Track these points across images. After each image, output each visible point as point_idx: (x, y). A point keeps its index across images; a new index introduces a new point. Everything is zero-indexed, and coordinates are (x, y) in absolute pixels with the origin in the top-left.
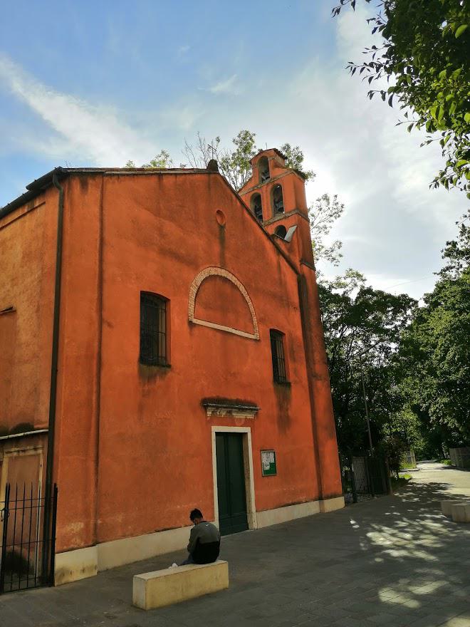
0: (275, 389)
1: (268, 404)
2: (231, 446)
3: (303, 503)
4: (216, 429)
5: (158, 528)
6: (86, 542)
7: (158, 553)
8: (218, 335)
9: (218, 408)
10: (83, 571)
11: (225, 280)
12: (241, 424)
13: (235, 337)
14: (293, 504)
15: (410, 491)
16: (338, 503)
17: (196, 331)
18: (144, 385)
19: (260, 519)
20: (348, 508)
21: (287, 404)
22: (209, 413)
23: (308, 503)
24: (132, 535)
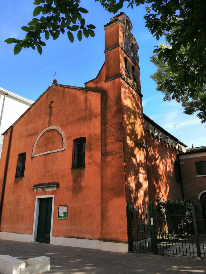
1: (67, 182)
2: (45, 204)
3: (86, 239)
4: (38, 197)
7: (13, 240)
11: (44, 133)
12: (49, 194)
13: (51, 154)
14: (78, 238)
15: (137, 179)
16: (123, 248)
17: (34, 159)
19: (55, 241)
21: (80, 179)
23: (92, 241)
24: (7, 232)
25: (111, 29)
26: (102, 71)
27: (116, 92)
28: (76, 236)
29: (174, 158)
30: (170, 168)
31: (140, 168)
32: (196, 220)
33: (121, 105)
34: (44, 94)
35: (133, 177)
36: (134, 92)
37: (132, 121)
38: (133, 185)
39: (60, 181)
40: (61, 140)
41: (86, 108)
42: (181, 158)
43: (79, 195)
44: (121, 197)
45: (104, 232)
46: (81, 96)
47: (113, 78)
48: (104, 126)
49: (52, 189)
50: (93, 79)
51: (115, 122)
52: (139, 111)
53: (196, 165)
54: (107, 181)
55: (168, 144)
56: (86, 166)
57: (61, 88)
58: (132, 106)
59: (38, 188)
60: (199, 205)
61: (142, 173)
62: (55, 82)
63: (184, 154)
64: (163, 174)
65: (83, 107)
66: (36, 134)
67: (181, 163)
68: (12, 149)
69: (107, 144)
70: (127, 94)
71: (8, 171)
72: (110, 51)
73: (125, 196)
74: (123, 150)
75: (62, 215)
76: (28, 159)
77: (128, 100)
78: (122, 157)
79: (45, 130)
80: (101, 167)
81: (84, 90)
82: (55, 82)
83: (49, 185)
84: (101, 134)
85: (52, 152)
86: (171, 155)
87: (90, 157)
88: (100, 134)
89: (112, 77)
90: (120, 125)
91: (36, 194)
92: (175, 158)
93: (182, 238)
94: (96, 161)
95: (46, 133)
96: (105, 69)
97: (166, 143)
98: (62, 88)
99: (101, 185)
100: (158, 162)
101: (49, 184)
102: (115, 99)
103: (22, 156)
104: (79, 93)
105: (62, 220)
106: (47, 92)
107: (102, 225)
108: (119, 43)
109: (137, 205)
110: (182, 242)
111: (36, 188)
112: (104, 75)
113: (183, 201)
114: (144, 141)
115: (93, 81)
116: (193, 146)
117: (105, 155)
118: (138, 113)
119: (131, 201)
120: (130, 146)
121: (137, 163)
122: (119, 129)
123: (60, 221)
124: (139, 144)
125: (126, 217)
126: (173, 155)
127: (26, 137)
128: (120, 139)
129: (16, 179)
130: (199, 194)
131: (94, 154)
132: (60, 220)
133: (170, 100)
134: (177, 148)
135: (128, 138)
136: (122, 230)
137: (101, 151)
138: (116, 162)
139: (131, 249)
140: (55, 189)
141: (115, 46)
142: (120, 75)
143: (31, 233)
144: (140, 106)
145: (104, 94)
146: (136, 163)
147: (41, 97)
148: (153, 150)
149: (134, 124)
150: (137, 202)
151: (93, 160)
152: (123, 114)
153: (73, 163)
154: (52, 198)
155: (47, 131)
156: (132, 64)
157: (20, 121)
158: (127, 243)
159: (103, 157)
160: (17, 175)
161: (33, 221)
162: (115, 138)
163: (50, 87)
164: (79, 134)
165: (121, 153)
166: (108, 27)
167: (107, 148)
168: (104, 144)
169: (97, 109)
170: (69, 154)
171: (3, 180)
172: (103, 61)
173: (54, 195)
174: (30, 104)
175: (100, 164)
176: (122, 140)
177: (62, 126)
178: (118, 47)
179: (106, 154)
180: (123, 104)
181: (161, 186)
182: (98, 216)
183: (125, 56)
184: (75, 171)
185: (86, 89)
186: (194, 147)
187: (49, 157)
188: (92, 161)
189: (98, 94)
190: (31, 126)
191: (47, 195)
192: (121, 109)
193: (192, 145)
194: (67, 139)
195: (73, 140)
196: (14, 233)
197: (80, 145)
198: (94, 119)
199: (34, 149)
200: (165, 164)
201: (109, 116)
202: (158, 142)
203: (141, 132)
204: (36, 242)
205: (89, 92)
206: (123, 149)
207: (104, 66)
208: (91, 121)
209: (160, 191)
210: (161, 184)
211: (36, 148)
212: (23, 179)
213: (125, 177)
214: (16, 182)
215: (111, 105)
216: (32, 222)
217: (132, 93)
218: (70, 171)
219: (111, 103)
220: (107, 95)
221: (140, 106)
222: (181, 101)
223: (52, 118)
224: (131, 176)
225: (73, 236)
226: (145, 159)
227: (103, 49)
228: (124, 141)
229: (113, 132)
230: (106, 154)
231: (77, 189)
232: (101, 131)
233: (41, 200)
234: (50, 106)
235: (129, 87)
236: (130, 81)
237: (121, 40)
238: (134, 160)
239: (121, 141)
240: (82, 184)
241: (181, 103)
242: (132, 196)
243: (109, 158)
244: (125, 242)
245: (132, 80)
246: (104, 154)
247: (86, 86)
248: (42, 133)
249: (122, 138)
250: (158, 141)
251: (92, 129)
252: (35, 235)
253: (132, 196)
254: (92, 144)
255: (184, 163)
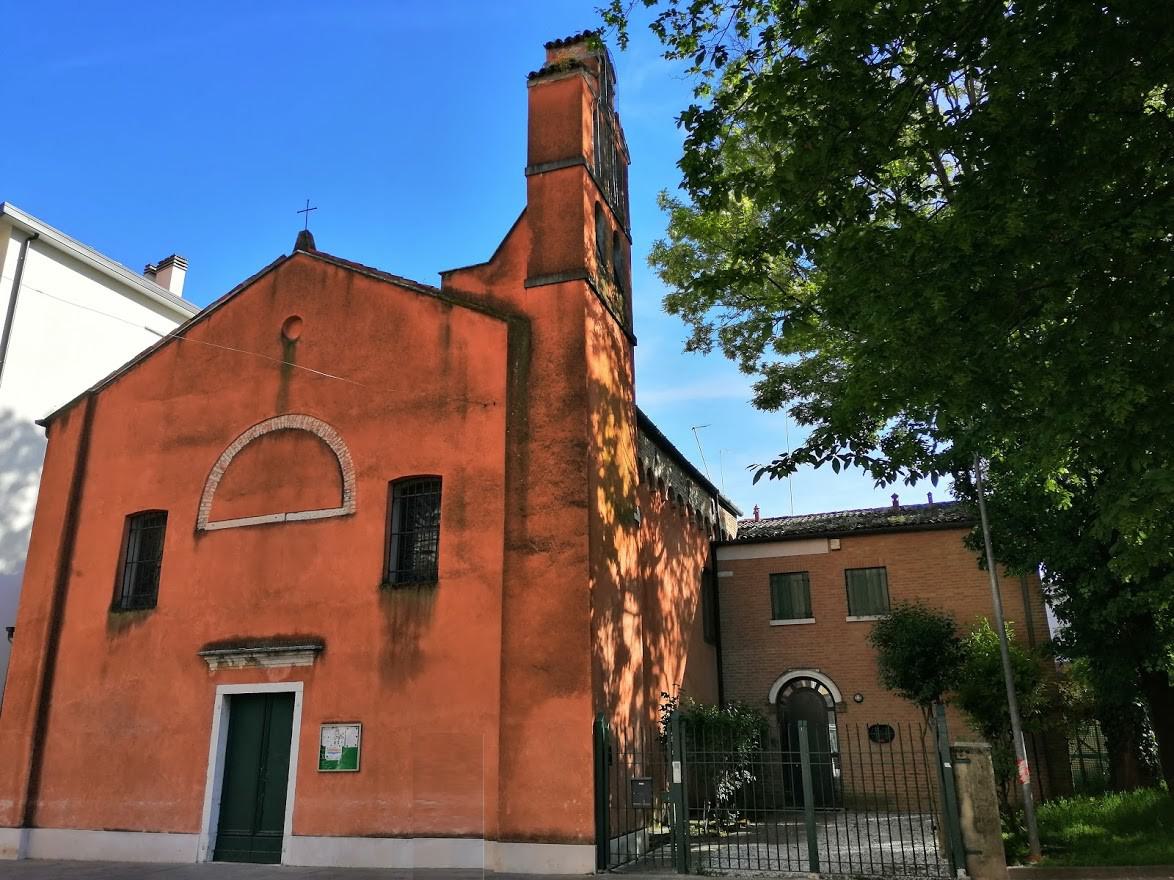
0: (381, 601)
5: (109, 827)
6: (13, 821)
8: (251, 534)
9: (222, 656)
10: (4, 851)
11: (254, 442)
13: (288, 527)
14: (405, 836)
15: (619, 631)
16: (583, 859)
17: (205, 542)
18: (112, 639)
20: (1002, 842)
22: (213, 666)
24: (75, 827)
25: (557, 91)
26: (514, 240)
27: (566, 330)
28: (396, 831)
29: (702, 554)
30: (691, 588)
31: (627, 596)
32: (812, 766)
33: (583, 377)
34: (254, 280)
35: (610, 627)
36: (616, 327)
37: (610, 433)
38: (609, 654)
39: (328, 628)
40: (332, 474)
41: (446, 368)
42: (724, 555)
43: (410, 684)
44: (576, 693)
45: (508, 812)
46: (425, 322)
47: (556, 278)
48: (520, 443)
49: (292, 661)
50: (478, 265)
51: (561, 435)
52: (627, 397)
53: (771, 584)
54: (527, 639)
55: (689, 506)
56: (440, 581)
57: (336, 273)
58: (611, 377)
59: (227, 654)
60: (773, 719)
61: (630, 613)
62: (305, 240)
63: (733, 543)
64: (671, 612)
65: (433, 362)
66: (219, 437)
67: (721, 574)
68: (91, 488)
69: (529, 511)
70: (601, 341)
71: (73, 580)
72: (548, 176)
73: (590, 691)
74: (586, 537)
75: (334, 755)
76: (175, 539)
77: (603, 357)
78: (583, 561)
79: (260, 430)
80: (505, 588)
81: (440, 298)
82: (305, 240)
83: (281, 645)
84: (506, 472)
85: (291, 517)
86: (695, 542)
87: (460, 551)
88: (502, 471)
89: (552, 274)
90: (578, 449)
91: (217, 679)
92: (705, 556)
93: (730, 829)
94: (483, 567)
95: (265, 441)
96: (525, 237)
97: (685, 503)
98: (342, 274)
99: (502, 651)
100: (660, 567)
101: (279, 640)
102: (563, 357)
103: (147, 527)
104: (415, 306)
105: (339, 776)
106: (271, 277)
107: (502, 788)
108: (584, 153)
109: (617, 719)
110: (729, 840)
111: (222, 656)
112: (522, 260)
113: (732, 710)
114: (638, 503)
115: (475, 272)
116: (756, 514)
117: (519, 547)
118: (626, 404)
119: (604, 706)
120: (606, 522)
121: (621, 577)
122: (574, 461)
123: (328, 780)
124: (626, 519)
125: (592, 759)
126: (699, 541)
127: (167, 447)
128: (576, 498)
129: (113, 615)
130: (775, 685)
131: (473, 543)
132: (329, 776)
133: (709, 350)
134: (713, 519)
135: (601, 493)
136: (574, 801)
137: (507, 533)
138: (559, 576)
139: (603, 860)
140: (305, 661)
141: (568, 158)
142: (583, 274)
143: (196, 828)
144: (630, 380)
145: (520, 331)
146: (618, 579)
147: (241, 289)
148: (650, 528)
149: (613, 443)
150: (617, 710)
151: (471, 564)
152: (590, 412)
153: (386, 569)
154: (291, 696)
155: (271, 434)
156: (614, 227)
157: (132, 378)
158: (591, 844)
159: (514, 554)
160: (119, 598)
161: (203, 782)
162: (559, 492)
163: (283, 260)
164: (415, 463)
165: (582, 545)
166: (542, 82)
167: (529, 525)
168: (517, 509)
169: (495, 381)
170: (373, 531)
171: (48, 615)
172: (522, 203)
173: (302, 683)
174: (182, 315)
175: (501, 579)
176: (583, 502)
177: (338, 421)
178: (578, 169)
179: (526, 546)
180: (590, 378)
181: (666, 653)
182: (490, 761)
183: (598, 197)
184: (393, 595)
185: (449, 296)
186: (762, 516)
187: (279, 538)
188: (466, 566)
189: (495, 323)
190: (187, 405)
191: (266, 680)
192: (582, 395)
193: (756, 508)
194: (360, 476)
195: (389, 482)
196: (106, 830)
197: (415, 501)
198: (475, 414)
199: (208, 500)
200: (678, 574)
201: (539, 413)
202: (662, 501)
203: (631, 469)
204: (214, 860)
205: (457, 310)
206: (587, 532)
207: (524, 223)
208: (464, 418)
209: (662, 670)
210: (665, 646)
211: (217, 495)
212: (150, 619)
213: (591, 630)
214: (116, 628)
215: (548, 375)
216: (196, 787)
217: (610, 333)
218: (374, 597)
219: (547, 366)
220: (531, 333)
221: (630, 380)
222: (738, 353)
223: (295, 385)
224: (605, 626)
225: (383, 829)
226: (638, 566)
227: (523, 162)
228: (590, 505)
229: (554, 472)
230: (526, 546)
231: (401, 661)
232: (508, 458)
233: (234, 701)
234: (283, 335)
235: (604, 314)
236: (608, 291)
237: (587, 143)
238: (614, 569)
239: (580, 504)
240: (423, 644)
241: (739, 360)
242: (607, 691)
243: (536, 561)
244: (586, 841)
245: (613, 287)
246: (517, 545)
247: (448, 284)
248: (245, 440)
249: (584, 496)
250: (663, 494)
251: (469, 450)
252: (210, 834)
253: (607, 691)
254: (469, 504)
255: (731, 574)
